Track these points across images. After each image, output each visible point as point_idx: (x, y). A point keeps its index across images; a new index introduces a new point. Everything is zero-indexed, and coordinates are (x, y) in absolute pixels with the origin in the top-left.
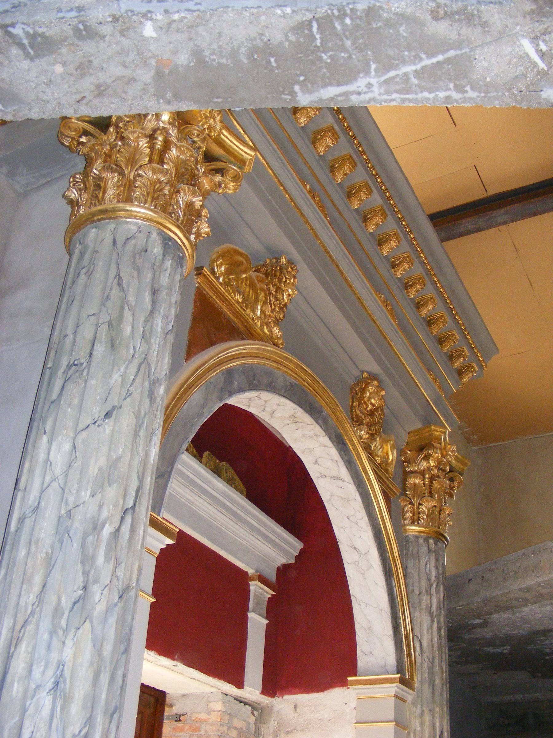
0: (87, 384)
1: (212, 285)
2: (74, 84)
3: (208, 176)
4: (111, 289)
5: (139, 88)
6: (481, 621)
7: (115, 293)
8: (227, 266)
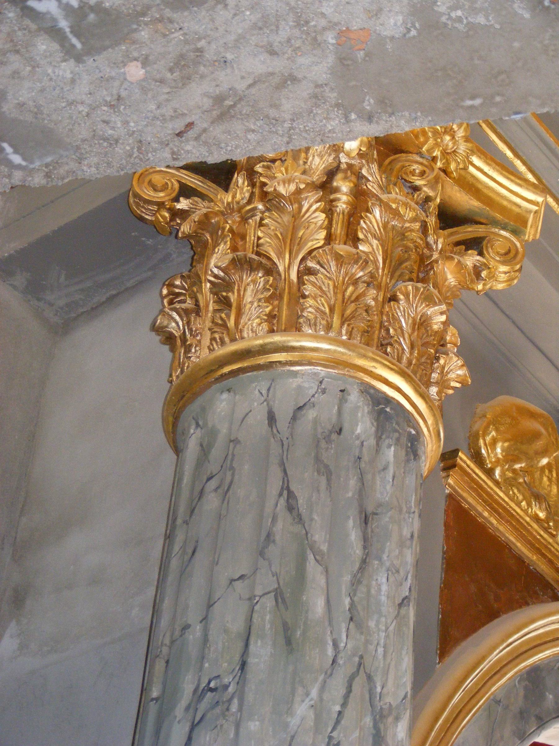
0: (241, 730)
1: (478, 488)
2: (168, 100)
3: (452, 258)
4: (274, 519)
5: (305, 94)
6: (298, 636)
7: (283, 527)
8: (506, 444)
